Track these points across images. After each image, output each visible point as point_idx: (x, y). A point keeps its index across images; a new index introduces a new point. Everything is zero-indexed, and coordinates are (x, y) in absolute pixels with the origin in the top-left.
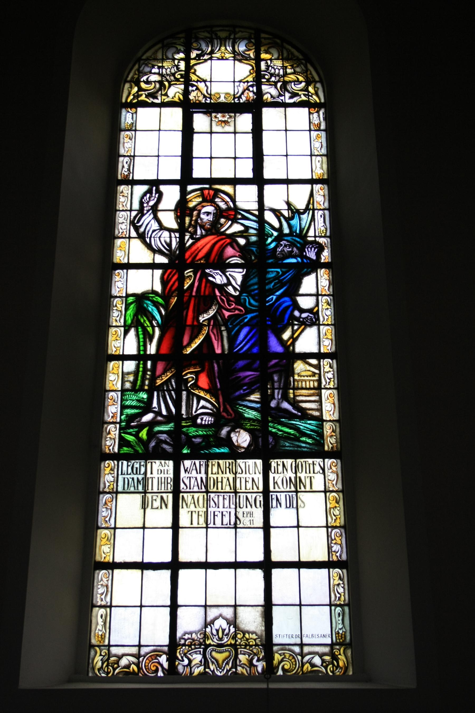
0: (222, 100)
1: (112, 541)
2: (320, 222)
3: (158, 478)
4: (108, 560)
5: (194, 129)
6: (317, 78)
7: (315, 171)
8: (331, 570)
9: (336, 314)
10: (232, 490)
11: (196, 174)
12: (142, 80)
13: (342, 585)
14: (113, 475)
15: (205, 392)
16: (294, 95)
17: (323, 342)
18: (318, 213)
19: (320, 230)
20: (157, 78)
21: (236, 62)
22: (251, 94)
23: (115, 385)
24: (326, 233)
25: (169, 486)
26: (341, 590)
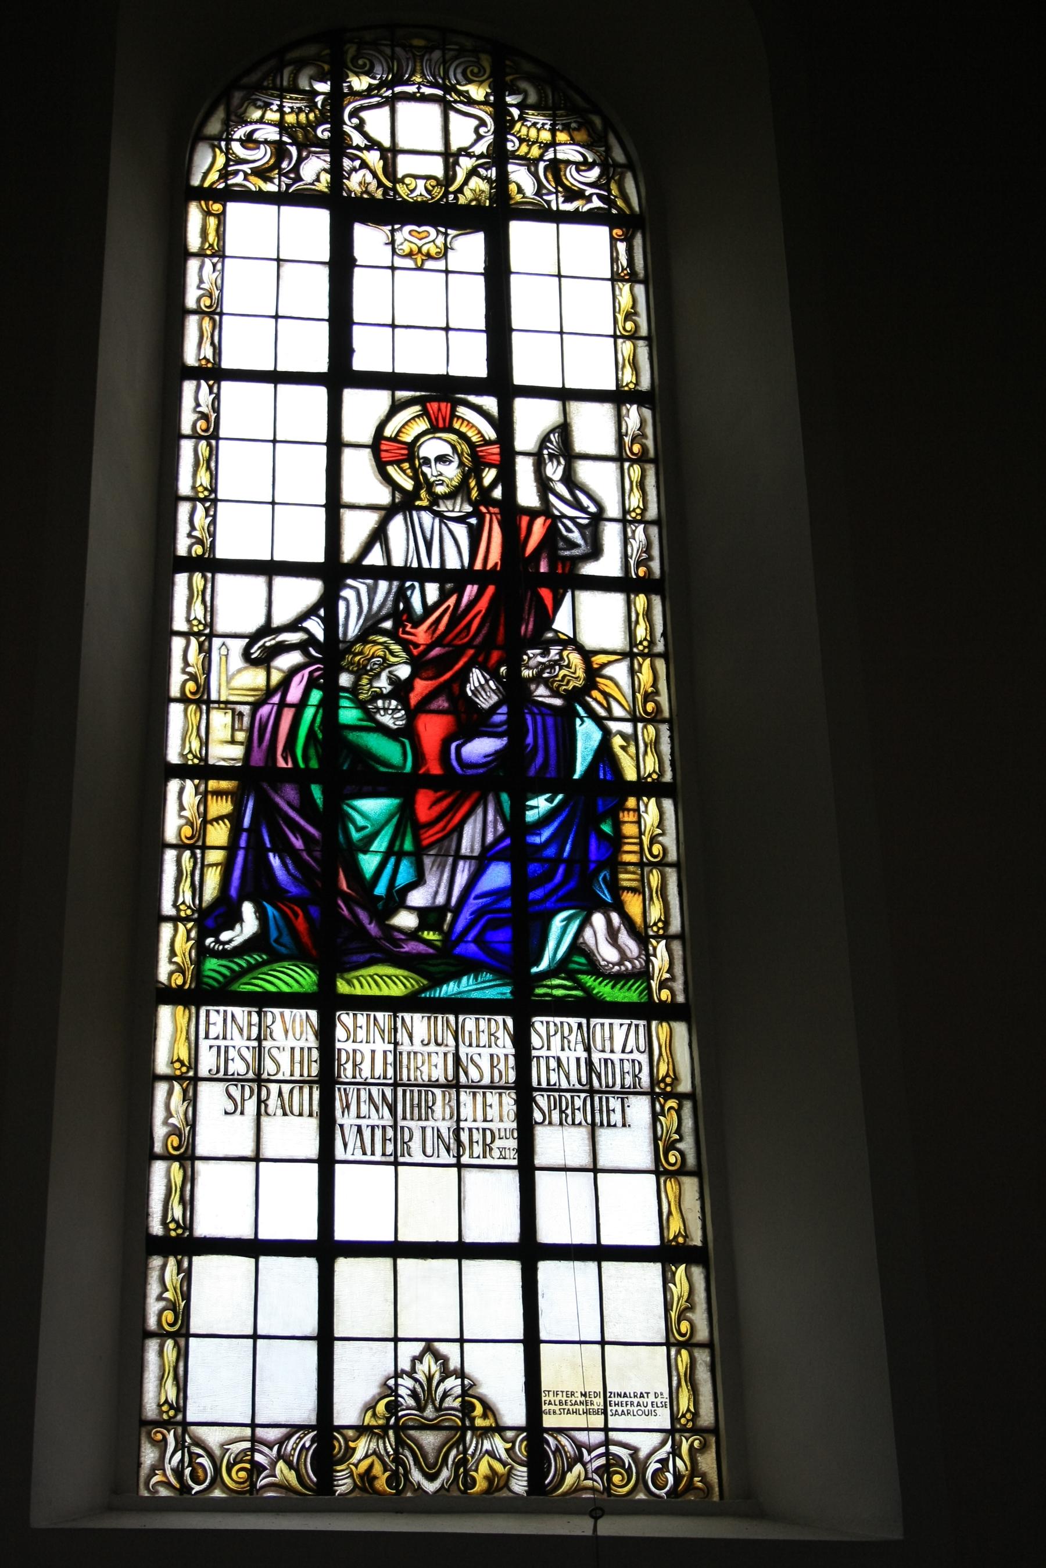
0: (421, 195)
3: (293, 1049)
5: (355, 260)
10: (251, 1075)
11: (360, 363)
12: (236, 136)
16: (572, 195)
20: (271, 133)
22: (484, 186)
25: (314, 1064)
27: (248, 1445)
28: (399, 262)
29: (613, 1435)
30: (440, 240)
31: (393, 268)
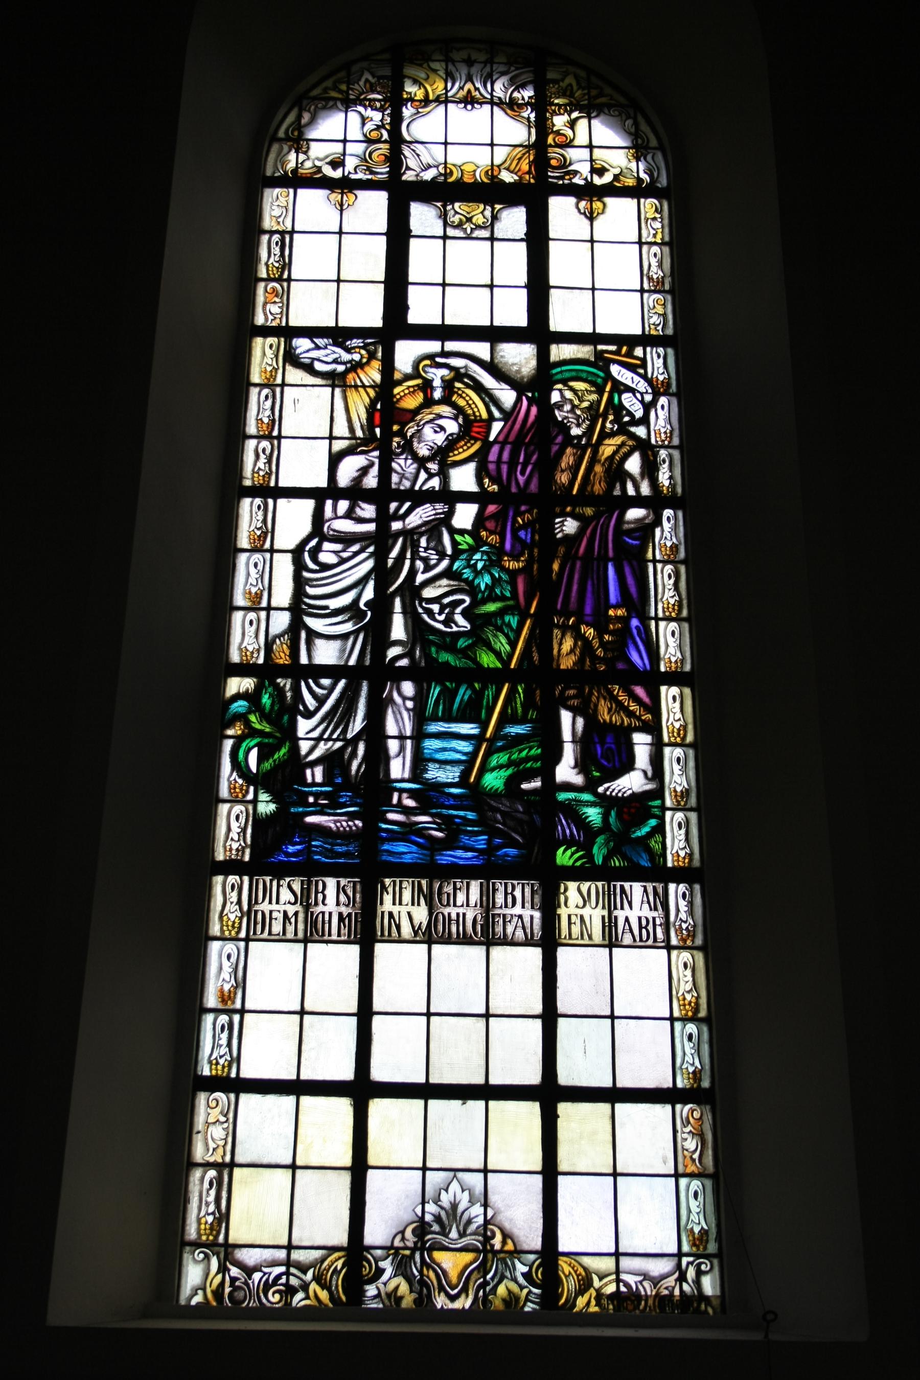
1: (231, 1115)
2: (656, 366)
4: (278, 324)
5: (411, 231)
6: (654, 142)
7: (662, 599)
8: (642, 200)
9: (714, 1041)
11: (415, 317)
13: (660, 220)
14: (226, 1125)
15: (414, 1225)
17: (649, 319)
18: (678, 957)
19: (673, 729)
21: (496, 108)
23: (281, 223)
24: (685, 735)
26: (657, 225)
27: (283, 1269)
28: (451, 232)
29: (625, 1262)
30: (488, 213)
31: (445, 237)
